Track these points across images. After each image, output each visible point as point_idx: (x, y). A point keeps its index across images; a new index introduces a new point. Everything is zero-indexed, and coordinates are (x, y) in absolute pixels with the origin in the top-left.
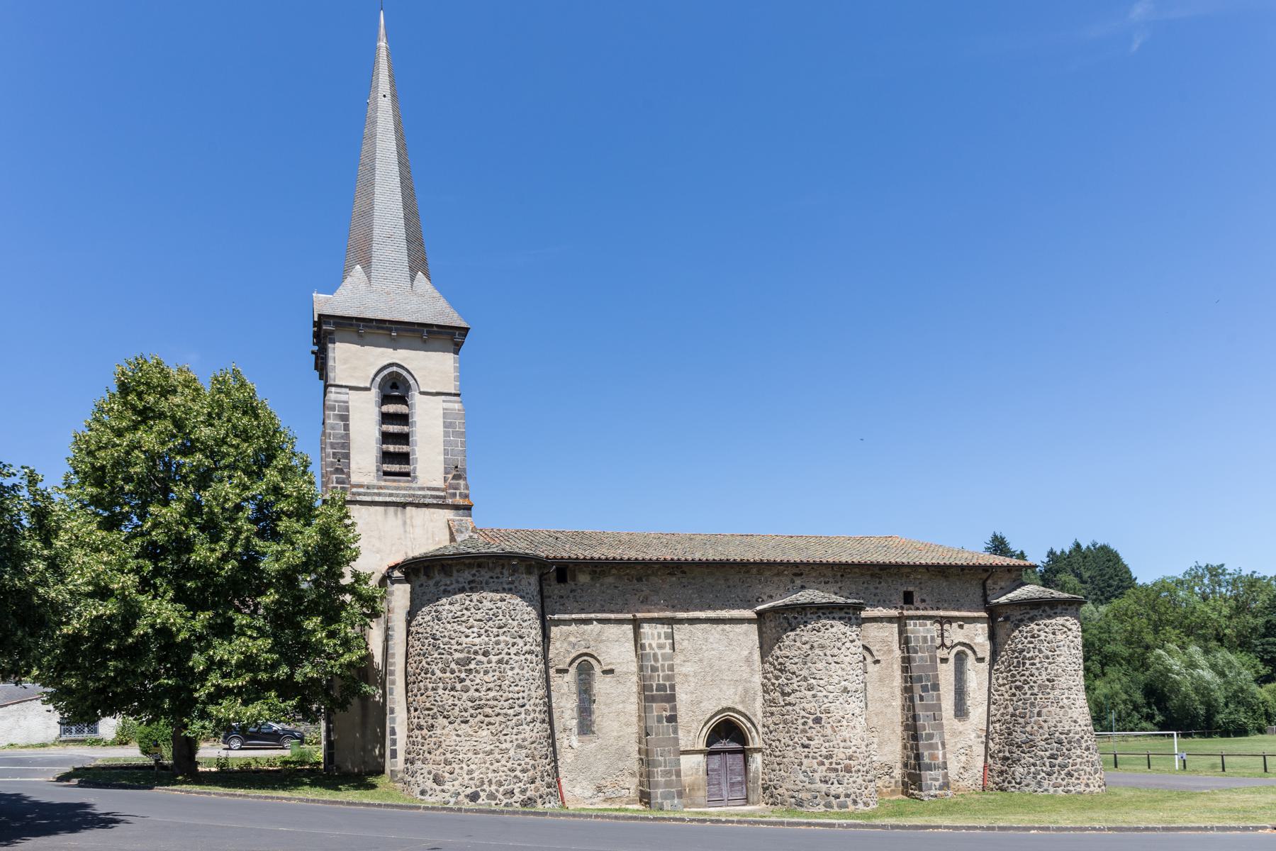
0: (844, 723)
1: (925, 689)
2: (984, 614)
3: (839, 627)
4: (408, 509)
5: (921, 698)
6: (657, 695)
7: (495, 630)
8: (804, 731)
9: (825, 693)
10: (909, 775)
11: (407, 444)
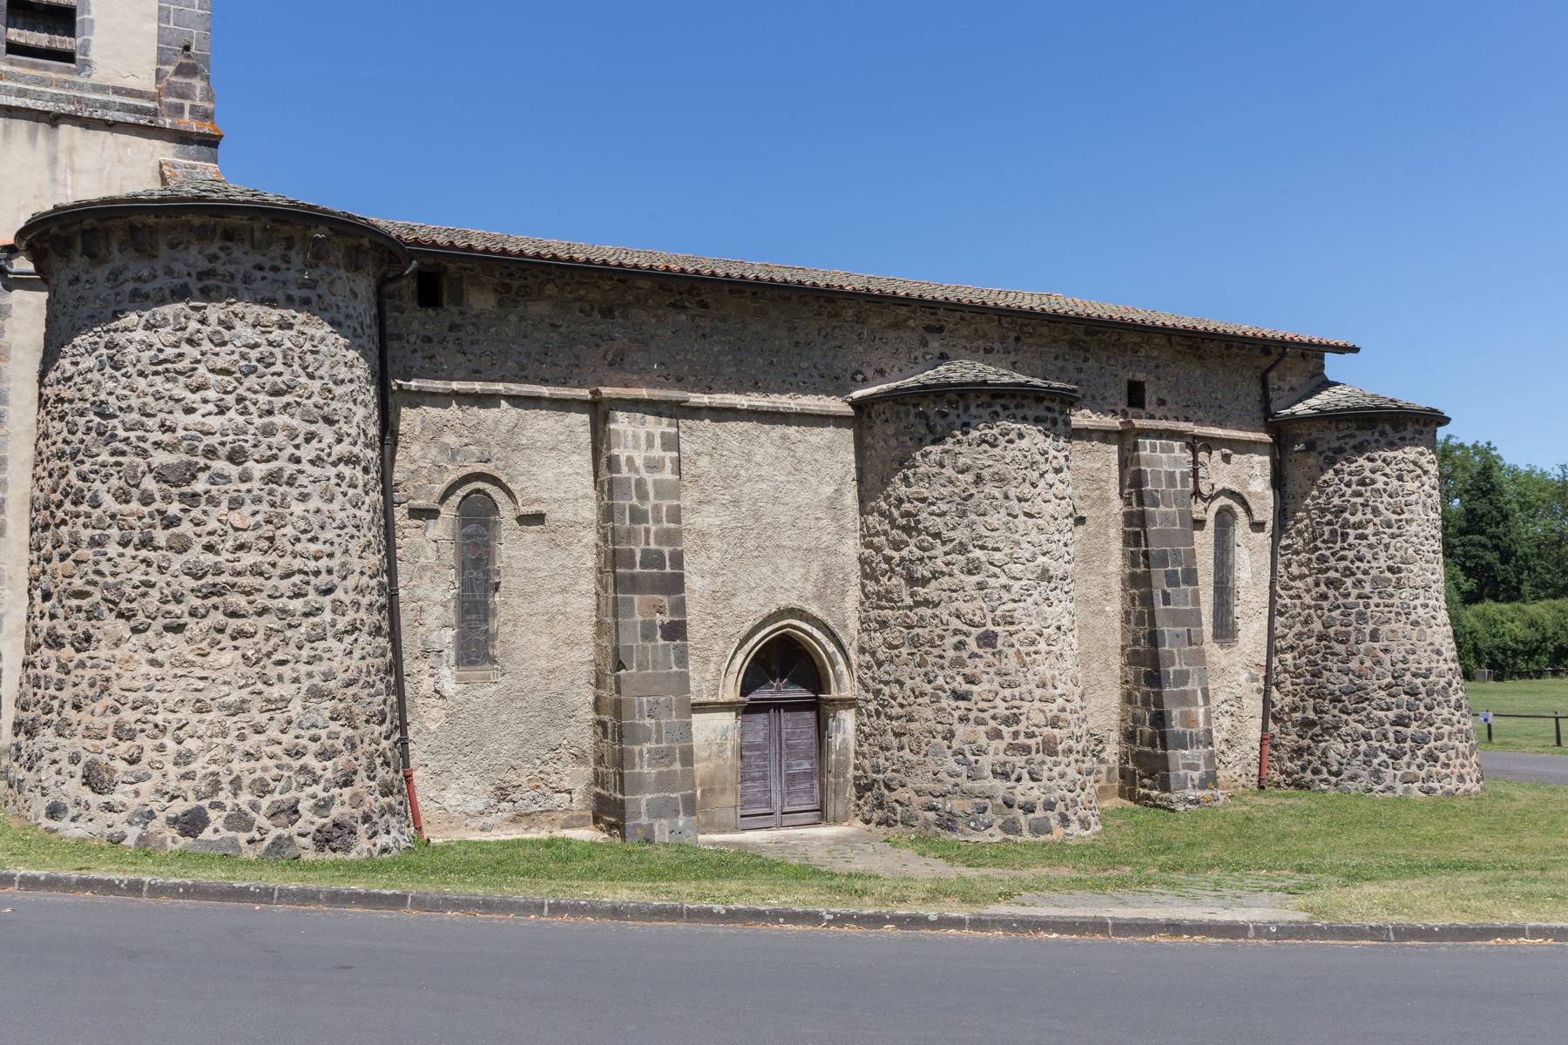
0: (1042, 646)
1: (1172, 579)
2: (1266, 437)
3: (1034, 439)
4: (65, 129)
5: (1167, 599)
6: (638, 573)
7: (263, 398)
8: (958, 662)
9: (1004, 580)
10: (1138, 758)
11: (70, 31)
